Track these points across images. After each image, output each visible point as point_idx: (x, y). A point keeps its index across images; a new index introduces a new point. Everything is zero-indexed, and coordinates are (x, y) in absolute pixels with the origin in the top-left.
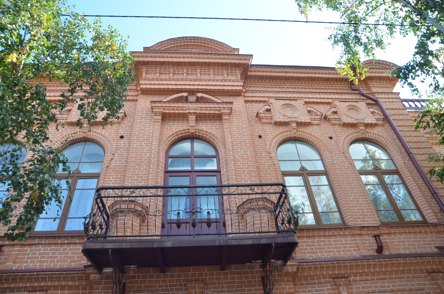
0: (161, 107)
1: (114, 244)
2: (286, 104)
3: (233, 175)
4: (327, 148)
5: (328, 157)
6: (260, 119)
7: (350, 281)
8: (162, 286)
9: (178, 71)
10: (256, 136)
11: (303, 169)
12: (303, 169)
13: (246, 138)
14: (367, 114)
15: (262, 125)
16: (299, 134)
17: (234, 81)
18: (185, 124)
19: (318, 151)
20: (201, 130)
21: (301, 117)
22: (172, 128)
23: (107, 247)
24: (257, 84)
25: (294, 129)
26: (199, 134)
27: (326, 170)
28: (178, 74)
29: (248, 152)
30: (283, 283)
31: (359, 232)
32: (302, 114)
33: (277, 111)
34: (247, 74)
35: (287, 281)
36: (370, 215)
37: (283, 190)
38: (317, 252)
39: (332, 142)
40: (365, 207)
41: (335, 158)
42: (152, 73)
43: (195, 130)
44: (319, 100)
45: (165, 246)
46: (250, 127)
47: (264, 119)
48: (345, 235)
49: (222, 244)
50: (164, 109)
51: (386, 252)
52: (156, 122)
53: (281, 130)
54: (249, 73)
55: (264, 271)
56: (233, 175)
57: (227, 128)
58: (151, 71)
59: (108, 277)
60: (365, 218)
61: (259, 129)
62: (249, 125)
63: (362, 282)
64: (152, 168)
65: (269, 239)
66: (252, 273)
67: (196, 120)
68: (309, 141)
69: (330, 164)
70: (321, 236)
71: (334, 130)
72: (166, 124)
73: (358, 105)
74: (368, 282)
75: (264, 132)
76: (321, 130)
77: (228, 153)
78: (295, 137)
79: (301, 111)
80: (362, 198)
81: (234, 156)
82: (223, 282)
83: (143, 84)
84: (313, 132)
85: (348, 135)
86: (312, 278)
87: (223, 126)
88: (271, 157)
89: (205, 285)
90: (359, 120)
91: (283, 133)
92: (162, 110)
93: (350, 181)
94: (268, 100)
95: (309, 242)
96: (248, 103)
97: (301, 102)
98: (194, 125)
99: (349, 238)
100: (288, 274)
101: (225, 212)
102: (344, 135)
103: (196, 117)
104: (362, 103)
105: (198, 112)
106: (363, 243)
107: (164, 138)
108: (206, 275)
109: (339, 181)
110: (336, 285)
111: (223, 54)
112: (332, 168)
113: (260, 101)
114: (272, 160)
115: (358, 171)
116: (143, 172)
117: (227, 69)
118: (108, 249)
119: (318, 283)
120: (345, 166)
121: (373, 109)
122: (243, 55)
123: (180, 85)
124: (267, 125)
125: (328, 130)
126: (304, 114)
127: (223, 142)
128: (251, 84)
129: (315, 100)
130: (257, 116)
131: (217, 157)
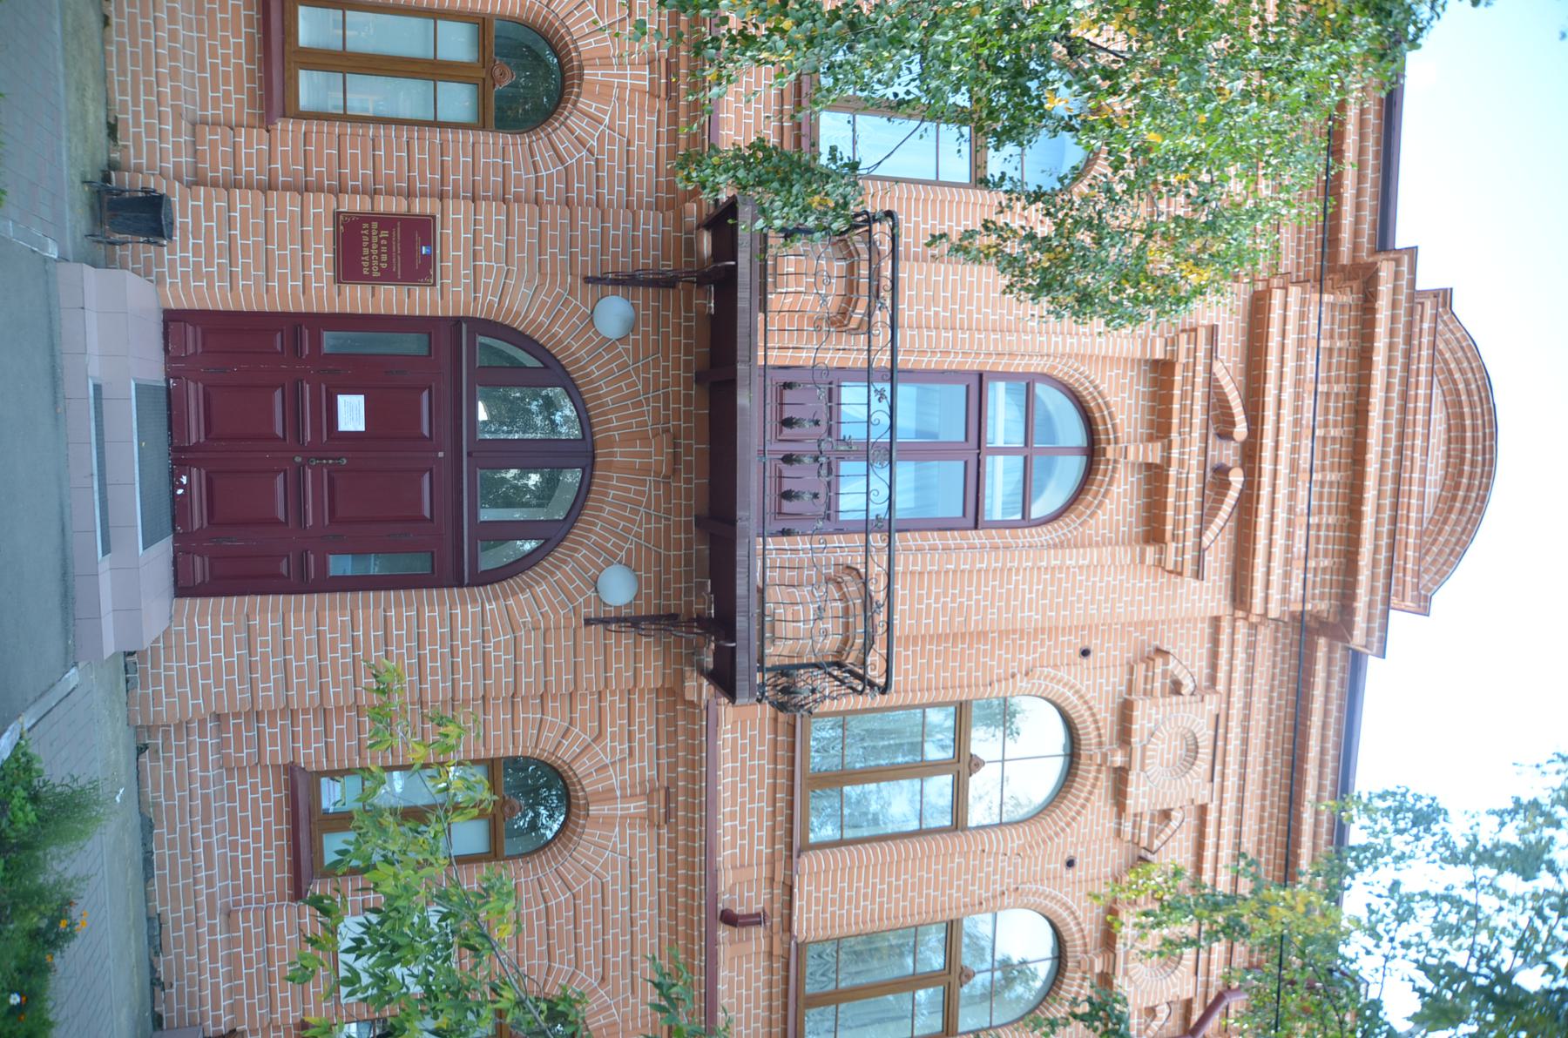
0: (1195, 357)
1: (748, 271)
2: (1197, 747)
3: (958, 565)
4: (1037, 844)
5: (1005, 840)
6: (1148, 659)
7: (659, 827)
8: (666, 375)
9: (1336, 408)
10: (1090, 641)
11: (975, 764)
12: (975, 764)
13: (1079, 609)
14: (1149, 993)
15: (1128, 663)
16: (1087, 770)
17: (1285, 588)
18: (1136, 430)
19: (1032, 818)
20: (1112, 478)
21: (1144, 785)
22: (1123, 392)
23: (739, 255)
24: (1283, 662)
25: (1105, 756)
26: (1101, 472)
27: (965, 828)
29: (1030, 610)
30: (660, 663)
31: (779, 877)
32: (1158, 792)
33: (1171, 713)
34: (1319, 633)
35: (664, 674)
36: (825, 920)
37: (872, 685)
38: (734, 760)
39: (1056, 862)
40: (849, 911)
41: (1003, 861)
42: (1333, 323)
43: (1116, 461)
44: (1209, 853)
45: (739, 392)
46: (1123, 625)
47: (1147, 670)
48: (773, 841)
49: (739, 524)
50: (1186, 366)
51: (723, 932)
52: (1144, 343)
53: (1105, 718)
54: (1322, 642)
55: (691, 620)
56: (958, 565)
57: (1113, 555)
58: (1342, 321)
59: (691, 247)
60: (817, 904)
61: (1112, 653)
62: (1130, 625)
63: (655, 854)
64: (987, 337)
65: (746, 634)
66: (688, 591)
67: (1149, 466)
68: (1065, 798)
69: (983, 843)
70: (775, 778)
71: (1099, 879)
72: (1138, 374)
73: (1182, 972)
74: (655, 869)
75: (1101, 667)
76: (1101, 840)
77: (1028, 555)
78: (1079, 756)
79: (1169, 788)
80: (873, 911)
81: (1018, 570)
82: (669, 520)
83: (1286, 296)
84: (1092, 814)
85: (1076, 918)
86: (672, 736)
87: (1123, 543)
88: (1013, 676)
89: (666, 477)
90: (1126, 962)
91: (1096, 722)
92: (1184, 361)
93: (928, 888)
94: (1216, 692)
95: (762, 744)
96: (1210, 627)
97: (1203, 796)
98: (1131, 457)
99: (766, 850)
100: (680, 677)
101: (816, 538)
102: (1079, 906)
103: (1158, 466)
104: (1191, 987)
105: (1173, 472)
106: (750, 882)
107: (1090, 369)
108: (688, 481)
109: (929, 857)
110: (652, 791)
111: (1390, 560)
112: (969, 846)
113: (1214, 666)
114: (1006, 679)
115: (959, 921)
116: (979, 312)
117: (1338, 569)
118: (735, 258)
119: (658, 750)
120: (973, 885)
121: (1164, 1016)
122: (1384, 628)
123: (1278, 415)
124: (1126, 677)
125: (1100, 861)
126: (1157, 796)
127: (1069, 540)
128: (1284, 644)
129: (1210, 841)
130: (1159, 651)
131: (1023, 523)
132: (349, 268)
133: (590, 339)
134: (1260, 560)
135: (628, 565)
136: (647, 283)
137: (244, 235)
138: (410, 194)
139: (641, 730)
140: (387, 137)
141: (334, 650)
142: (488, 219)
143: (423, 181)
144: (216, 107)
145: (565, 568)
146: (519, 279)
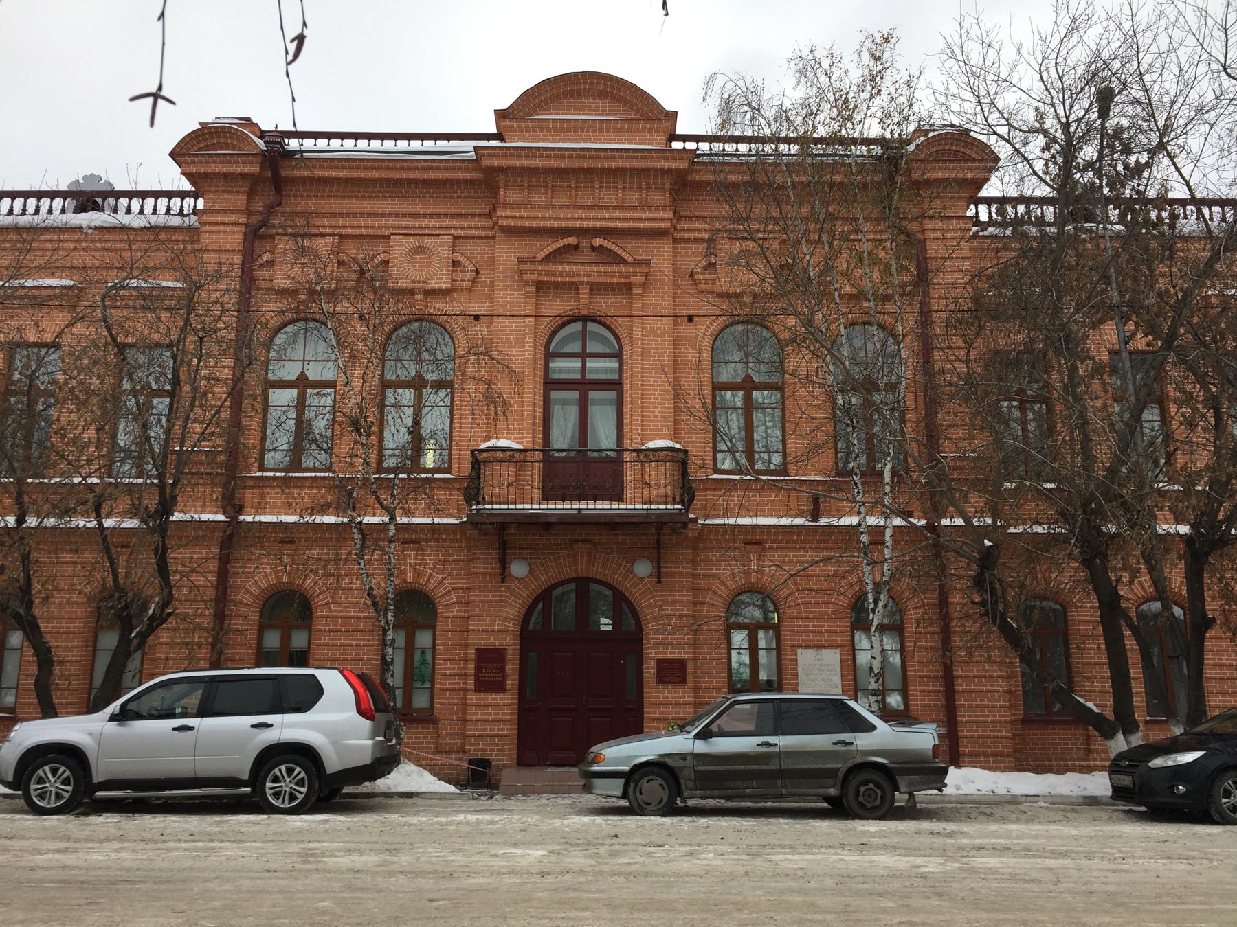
6: (696, 283)
11: (302, 377)
12: (302, 377)
28: (561, 187)
52: (528, 297)
103: (591, 290)
105: (593, 280)
132: (499, 686)
133: (530, 580)
134: (641, 225)
135: (633, 563)
136: (504, 554)
137: (486, 730)
138: (466, 660)
139: (716, 556)
140: (440, 669)
141: (668, 697)
142: (478, 625)
143: (460, 654)
144: (429, 743)
145: (636, 594)
146: (503, 611)
